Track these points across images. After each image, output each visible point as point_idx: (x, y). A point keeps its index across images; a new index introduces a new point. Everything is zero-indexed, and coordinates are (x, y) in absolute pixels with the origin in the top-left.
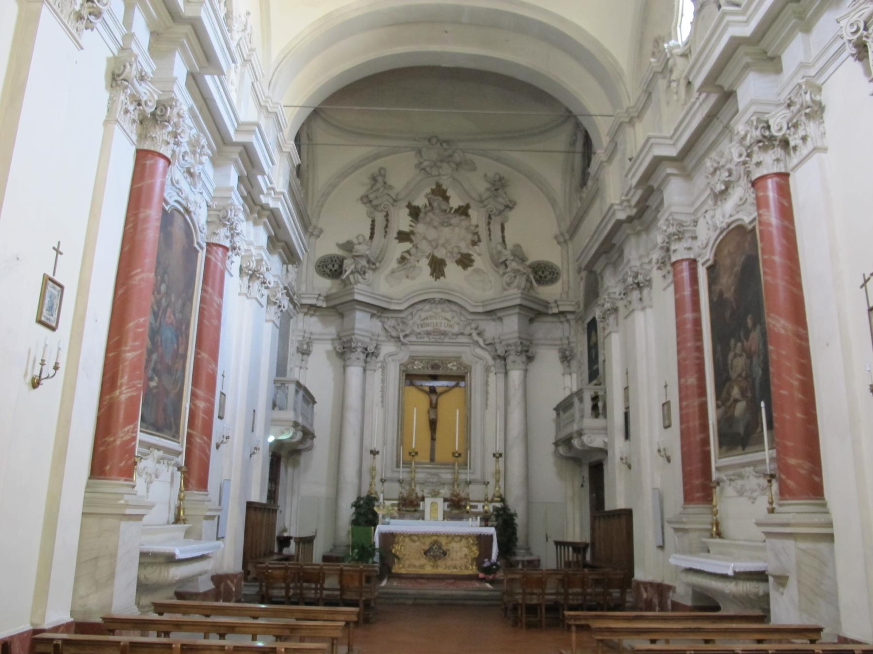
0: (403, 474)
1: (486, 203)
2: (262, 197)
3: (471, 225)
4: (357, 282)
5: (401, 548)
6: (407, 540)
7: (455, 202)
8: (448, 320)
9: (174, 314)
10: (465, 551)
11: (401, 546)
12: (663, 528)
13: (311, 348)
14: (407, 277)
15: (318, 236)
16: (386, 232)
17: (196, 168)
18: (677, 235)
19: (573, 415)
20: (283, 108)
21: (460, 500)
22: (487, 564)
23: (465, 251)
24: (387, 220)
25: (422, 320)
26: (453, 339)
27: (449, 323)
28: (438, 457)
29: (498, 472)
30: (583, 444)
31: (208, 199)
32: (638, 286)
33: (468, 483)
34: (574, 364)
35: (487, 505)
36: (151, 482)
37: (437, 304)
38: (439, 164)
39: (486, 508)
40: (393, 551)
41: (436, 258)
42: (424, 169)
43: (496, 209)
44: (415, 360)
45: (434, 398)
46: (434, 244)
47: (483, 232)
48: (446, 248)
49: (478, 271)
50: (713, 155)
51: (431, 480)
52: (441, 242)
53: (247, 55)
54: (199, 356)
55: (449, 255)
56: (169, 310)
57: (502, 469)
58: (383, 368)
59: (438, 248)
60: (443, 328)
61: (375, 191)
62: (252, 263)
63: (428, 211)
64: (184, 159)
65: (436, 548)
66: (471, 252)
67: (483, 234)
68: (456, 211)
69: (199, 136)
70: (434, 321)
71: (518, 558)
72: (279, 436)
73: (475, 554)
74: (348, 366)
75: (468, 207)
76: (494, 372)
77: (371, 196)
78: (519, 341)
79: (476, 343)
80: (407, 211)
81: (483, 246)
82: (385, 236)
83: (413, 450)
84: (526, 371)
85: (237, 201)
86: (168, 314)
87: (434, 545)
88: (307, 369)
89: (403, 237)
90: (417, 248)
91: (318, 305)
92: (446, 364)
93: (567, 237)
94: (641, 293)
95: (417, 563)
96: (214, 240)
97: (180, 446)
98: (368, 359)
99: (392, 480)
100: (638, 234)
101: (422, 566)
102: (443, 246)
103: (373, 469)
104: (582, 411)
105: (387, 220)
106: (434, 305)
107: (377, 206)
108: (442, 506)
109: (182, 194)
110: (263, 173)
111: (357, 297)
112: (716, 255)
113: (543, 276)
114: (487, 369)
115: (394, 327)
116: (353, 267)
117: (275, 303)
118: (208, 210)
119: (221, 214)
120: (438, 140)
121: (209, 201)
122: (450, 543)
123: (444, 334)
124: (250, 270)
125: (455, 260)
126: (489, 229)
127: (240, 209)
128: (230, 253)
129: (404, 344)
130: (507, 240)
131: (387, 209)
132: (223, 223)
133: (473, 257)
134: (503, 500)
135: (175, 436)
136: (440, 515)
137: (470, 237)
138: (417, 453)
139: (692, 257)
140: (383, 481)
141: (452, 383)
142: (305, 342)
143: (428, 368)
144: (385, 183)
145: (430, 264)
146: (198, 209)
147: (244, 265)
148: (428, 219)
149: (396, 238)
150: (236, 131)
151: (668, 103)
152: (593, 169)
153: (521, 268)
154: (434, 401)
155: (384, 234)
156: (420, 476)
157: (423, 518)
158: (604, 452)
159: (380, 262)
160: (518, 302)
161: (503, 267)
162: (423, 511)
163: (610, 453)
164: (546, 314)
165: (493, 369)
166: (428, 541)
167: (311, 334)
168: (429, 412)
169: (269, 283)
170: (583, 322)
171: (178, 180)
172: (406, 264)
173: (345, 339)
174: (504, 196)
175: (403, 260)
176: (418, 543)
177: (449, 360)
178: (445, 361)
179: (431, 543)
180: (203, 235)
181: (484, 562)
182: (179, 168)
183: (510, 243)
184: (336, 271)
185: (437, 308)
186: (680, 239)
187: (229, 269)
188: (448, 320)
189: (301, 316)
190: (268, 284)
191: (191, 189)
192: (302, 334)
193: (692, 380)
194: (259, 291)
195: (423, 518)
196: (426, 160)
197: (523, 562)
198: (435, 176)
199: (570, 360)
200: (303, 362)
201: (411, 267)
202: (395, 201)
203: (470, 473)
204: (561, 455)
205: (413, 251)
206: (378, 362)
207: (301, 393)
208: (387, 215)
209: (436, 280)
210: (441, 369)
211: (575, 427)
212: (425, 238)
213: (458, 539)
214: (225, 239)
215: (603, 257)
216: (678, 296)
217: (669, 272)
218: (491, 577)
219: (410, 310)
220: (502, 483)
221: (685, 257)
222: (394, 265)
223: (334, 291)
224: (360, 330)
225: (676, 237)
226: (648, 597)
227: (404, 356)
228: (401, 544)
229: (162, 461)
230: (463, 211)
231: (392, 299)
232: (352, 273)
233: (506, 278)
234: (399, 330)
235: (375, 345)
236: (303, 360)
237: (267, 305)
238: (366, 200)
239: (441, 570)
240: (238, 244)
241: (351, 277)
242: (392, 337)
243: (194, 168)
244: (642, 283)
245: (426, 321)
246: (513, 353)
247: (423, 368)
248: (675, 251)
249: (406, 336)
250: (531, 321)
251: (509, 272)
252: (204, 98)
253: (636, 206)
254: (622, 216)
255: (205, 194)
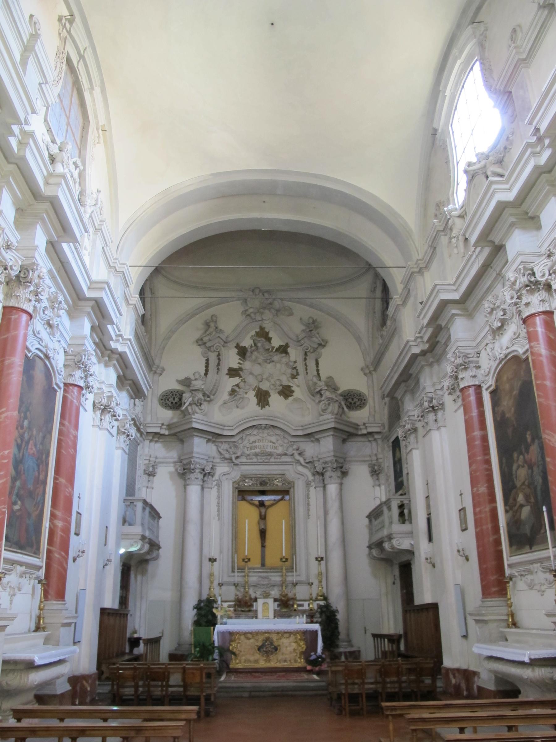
0: (237, 578)
1: (302, 342)
2: (111, 343)
3: (290, 361)
4: (195, 412)
5: (237, 645)
6: (242, 637)
7: (276, 342)
8: (273, 443)
9: (35, 445)
10: (294, 645)
11: (238, 643)
12: (465, 619)
13: (156, 470)
14: (237, 407)
15: (161, 374)
16: (218, 369)
17: (55, 321)
18: (463, 365)
19: (383, 522)
20: (129, 267)
21: (289, 600)
22: (313, 657)
23: (285, 383)
24: (219, 359)
25: (250, 443)
26: (277, 459)
27: (273, 445)
28: (268, 562)
29: (320, 574)
30: (393, 547)
31: (66, 346)
32: (434, 409)
33: (295, 584)
34: (382, 477)
35: (312, 603)
36: (14, 595)
37: (263, 429)
38: (262, 310)
39: (311, 606)
40: (231, 648)
41: (262, 389)
42: (249, 315)
43: (310, 346)
44: (246, 478)
45: (263, 510)
46: (259, 377)
47: (300, 367)
48: (269, 381)
49: (297, 400)
50: (490, 298)
51: (262, 583)
52: (265, 376)
53: (99, 225)
54: (58, 482)
55: (272, 387)
56: (31, 442)
57: (324, 571)
58: (219, 485)
59: (263, 381)
60: (269, 450)
61: (208, 335)
62: (103, 399)
63: (254, 351)
64: (44, 313)
65: (268, 645)
66: (291, 384)
67: (301, 368)
68: (277, 350)
69: (57, 293)
70: (261, 444)
71: (341, 650)
72: (129, 548)
73: (303, 648)
74: (188, 485)
75: (287, 346)
76: (314, 486)
77: (205, 339)
78: (334, 459)
79: (298, 461)
80: (236, 351)
81: (301, 378)
82: (218, 372)
83: (246, 556)
84: (341, 484)
85: (90, 346)
86: (30, 446)
87: (266, 642)
88: (153, 488)
89: (233, 372)
90: (245, 382)
91: (162, 433)
92: (273, 481)
93: (372, 369)
94: (436, 415)
95: (252, 658)
96: (71, 381)
97: (41, 561)
98: (206, 479)
99: (228, 584)
100: (431, 365)
101: (256, 661)
102: (267, 379)
103: (211, 575)
104: (391, 517)
105: (219, 359)
106: (261, 431)
107: (210, 347)
108: (272, 606)
109: (42, 343)
110: (112, 323)
111: (195, 425)
112: (497, 381)
113: (353, 402)
114: (308, 484)
115: (227, 450)
116: (191, 399)
117: (124, 433)
118: (65, 356)
119: (76, 359)
120: (260, 291)
121: (66, 348)
122: (281, 639)
123: (270, 455)
124: (101, 405)
125: (277, 391)
126: (306, 364)
127: (92, 354)
128: (84, 392)
129: (236, 465)
130: (320, 372)
131: (218, 350)
132: (78, 366)
133: (292, 389)
134: (325, 599)
135: (36, 552)
136: (271, 614)
137: (289, 371)
138: (249, 560)
139: (477, 383)
140: (220, 585)
141: (278, 497)
142: (151, 465)
143: (257, 484)
144: (216, 328)
145: (257, 395)
146: (56, 355)
147: (97, 402)
148: (254, 357)
149: (227, 374)
150: (89, 288)
151: (450, 256)
152: (391, 311)
153: (333, 396)
154: (263, 514)
155: (217, 371)
156: (253, 579)
157: (256, 617)
158: (411, 553)
159: (214, 395)
160: (332, 425)
161: (318, 396)
162: (256, 611)
163: (416, 554)
164: (357, 435)
165: (313, 483)
166: (261, 638)
167: (156, 458)
168: (259, 523)
169: (119, 416)
170: (388, 441)
171: (39, 331)
172: (235, 396)
173: (185, 462)
174: (317, 336)
175: (233, 392)
176: (252, 641)
177: (275, 477)
178: (270, 478)
179: (263, 640)
180: (61, 377)
181: (311, 656)
182: (40, 320)
183: (323, 376)
184: (176, 403)
185: (263, 433)
186: (466, 369)
187: (84, 405)
188: (273, 443)
189: (147, 442)
190: (118, 417)
191: (50, 338)
192: (148, 458)
193: (483, 489)
194: (110, 423)
195: (256, 617)
196: (251, 308)
197: (345, 653)
198: (259, 321)
199: (379, 474)
200: (150, 482)
201: (241, 398)
202: (225, 342)
203: (297, 576)
204: (375, 557)
205: (242, 385)
206: (214, 481)
207: (148, 510)
208: (219, 355)
209: (262, 409)
210: (268, 485)
211: (385, 532)
212: (251, 373)
213: (287, 635)
214: (80, 379)
215: (403, 385)
216: (467, 417)
217: (458, 397)
218: (317, 669)
219: (240, 436)
220: (324, 583)
221: (471, 384)
222: (225, 396)
223: (175, 420)
224: (197, 453)
225: (463, 367)
226: (456, 682)
227: (236, 475)
228: (237, 641)
229: (24, 576)
230: (283, 350)
231: (224, 426)
232: (190, 404)
233: (322, 406)
234: (232, 453)
235: (211, 466)
236: (149, 481)
237: (117, 435)
238: (200, 342)
239: (273, 664)
240: (91, 384)
241: (189, 408)
242: (227, 459)
243: (53, 321)
244: (437, 407)
245: (254, 444)
246: (329, 469)
247: (253, 484)
248: (462, 379)
249: (237, 458)
250: (344, 441)
251: (324, 400)
252: (61, 262)
253: (427, 342)
254: (416, 350)
255: (62, 342)
